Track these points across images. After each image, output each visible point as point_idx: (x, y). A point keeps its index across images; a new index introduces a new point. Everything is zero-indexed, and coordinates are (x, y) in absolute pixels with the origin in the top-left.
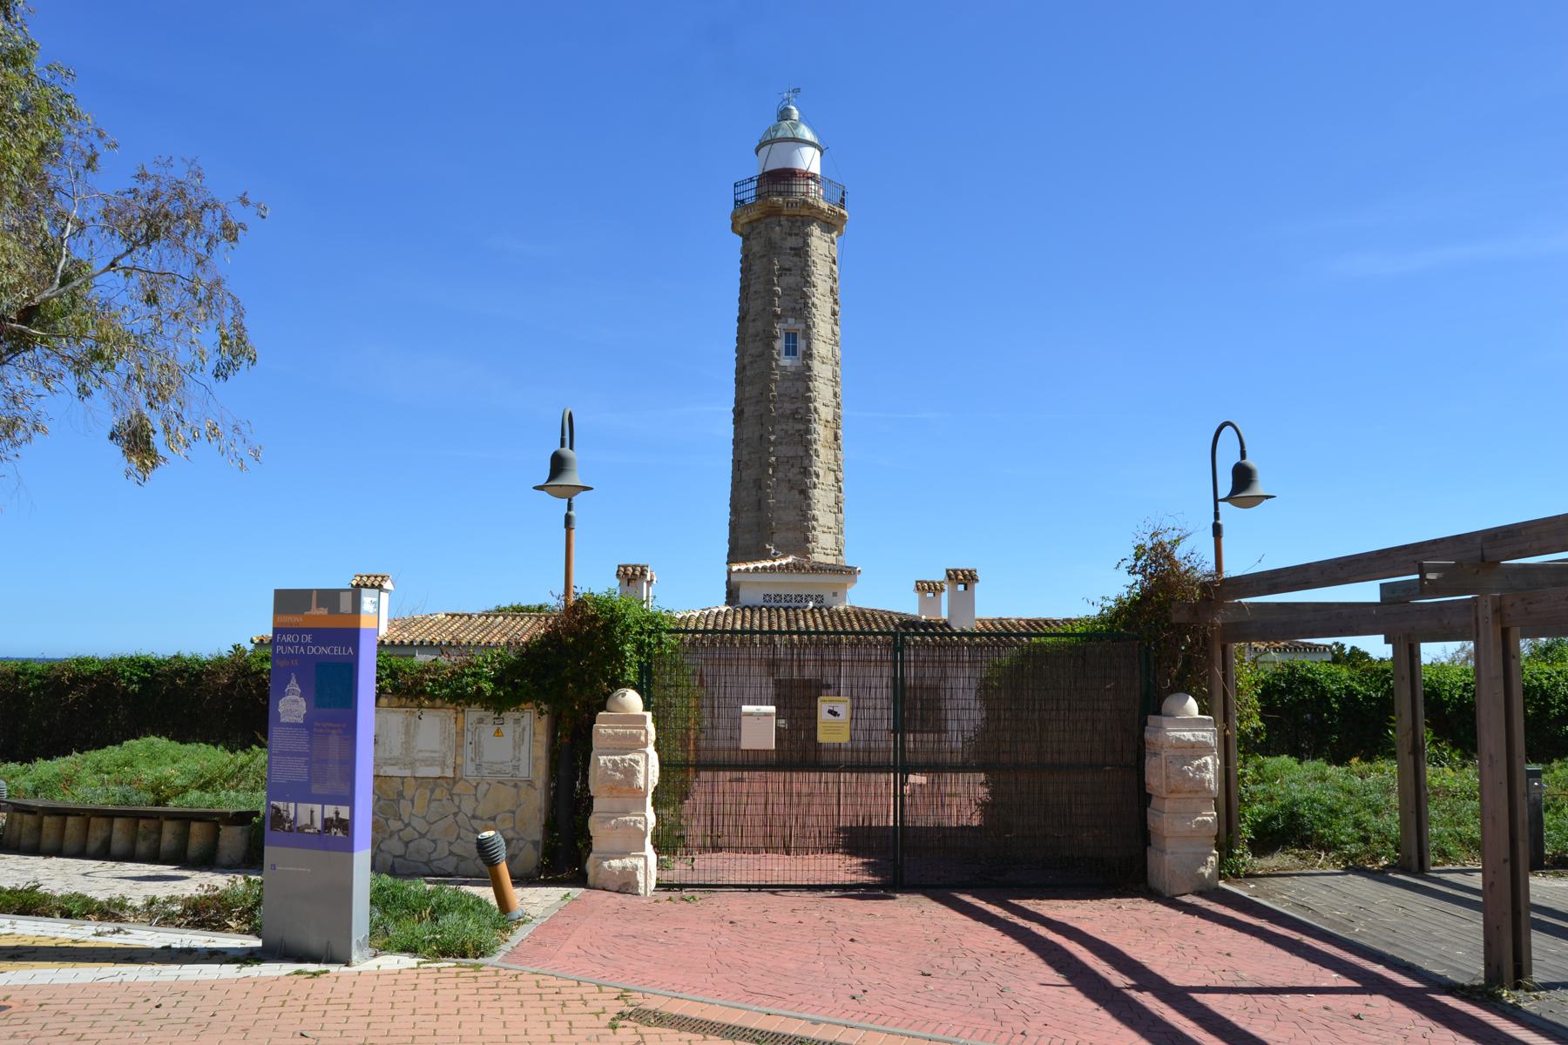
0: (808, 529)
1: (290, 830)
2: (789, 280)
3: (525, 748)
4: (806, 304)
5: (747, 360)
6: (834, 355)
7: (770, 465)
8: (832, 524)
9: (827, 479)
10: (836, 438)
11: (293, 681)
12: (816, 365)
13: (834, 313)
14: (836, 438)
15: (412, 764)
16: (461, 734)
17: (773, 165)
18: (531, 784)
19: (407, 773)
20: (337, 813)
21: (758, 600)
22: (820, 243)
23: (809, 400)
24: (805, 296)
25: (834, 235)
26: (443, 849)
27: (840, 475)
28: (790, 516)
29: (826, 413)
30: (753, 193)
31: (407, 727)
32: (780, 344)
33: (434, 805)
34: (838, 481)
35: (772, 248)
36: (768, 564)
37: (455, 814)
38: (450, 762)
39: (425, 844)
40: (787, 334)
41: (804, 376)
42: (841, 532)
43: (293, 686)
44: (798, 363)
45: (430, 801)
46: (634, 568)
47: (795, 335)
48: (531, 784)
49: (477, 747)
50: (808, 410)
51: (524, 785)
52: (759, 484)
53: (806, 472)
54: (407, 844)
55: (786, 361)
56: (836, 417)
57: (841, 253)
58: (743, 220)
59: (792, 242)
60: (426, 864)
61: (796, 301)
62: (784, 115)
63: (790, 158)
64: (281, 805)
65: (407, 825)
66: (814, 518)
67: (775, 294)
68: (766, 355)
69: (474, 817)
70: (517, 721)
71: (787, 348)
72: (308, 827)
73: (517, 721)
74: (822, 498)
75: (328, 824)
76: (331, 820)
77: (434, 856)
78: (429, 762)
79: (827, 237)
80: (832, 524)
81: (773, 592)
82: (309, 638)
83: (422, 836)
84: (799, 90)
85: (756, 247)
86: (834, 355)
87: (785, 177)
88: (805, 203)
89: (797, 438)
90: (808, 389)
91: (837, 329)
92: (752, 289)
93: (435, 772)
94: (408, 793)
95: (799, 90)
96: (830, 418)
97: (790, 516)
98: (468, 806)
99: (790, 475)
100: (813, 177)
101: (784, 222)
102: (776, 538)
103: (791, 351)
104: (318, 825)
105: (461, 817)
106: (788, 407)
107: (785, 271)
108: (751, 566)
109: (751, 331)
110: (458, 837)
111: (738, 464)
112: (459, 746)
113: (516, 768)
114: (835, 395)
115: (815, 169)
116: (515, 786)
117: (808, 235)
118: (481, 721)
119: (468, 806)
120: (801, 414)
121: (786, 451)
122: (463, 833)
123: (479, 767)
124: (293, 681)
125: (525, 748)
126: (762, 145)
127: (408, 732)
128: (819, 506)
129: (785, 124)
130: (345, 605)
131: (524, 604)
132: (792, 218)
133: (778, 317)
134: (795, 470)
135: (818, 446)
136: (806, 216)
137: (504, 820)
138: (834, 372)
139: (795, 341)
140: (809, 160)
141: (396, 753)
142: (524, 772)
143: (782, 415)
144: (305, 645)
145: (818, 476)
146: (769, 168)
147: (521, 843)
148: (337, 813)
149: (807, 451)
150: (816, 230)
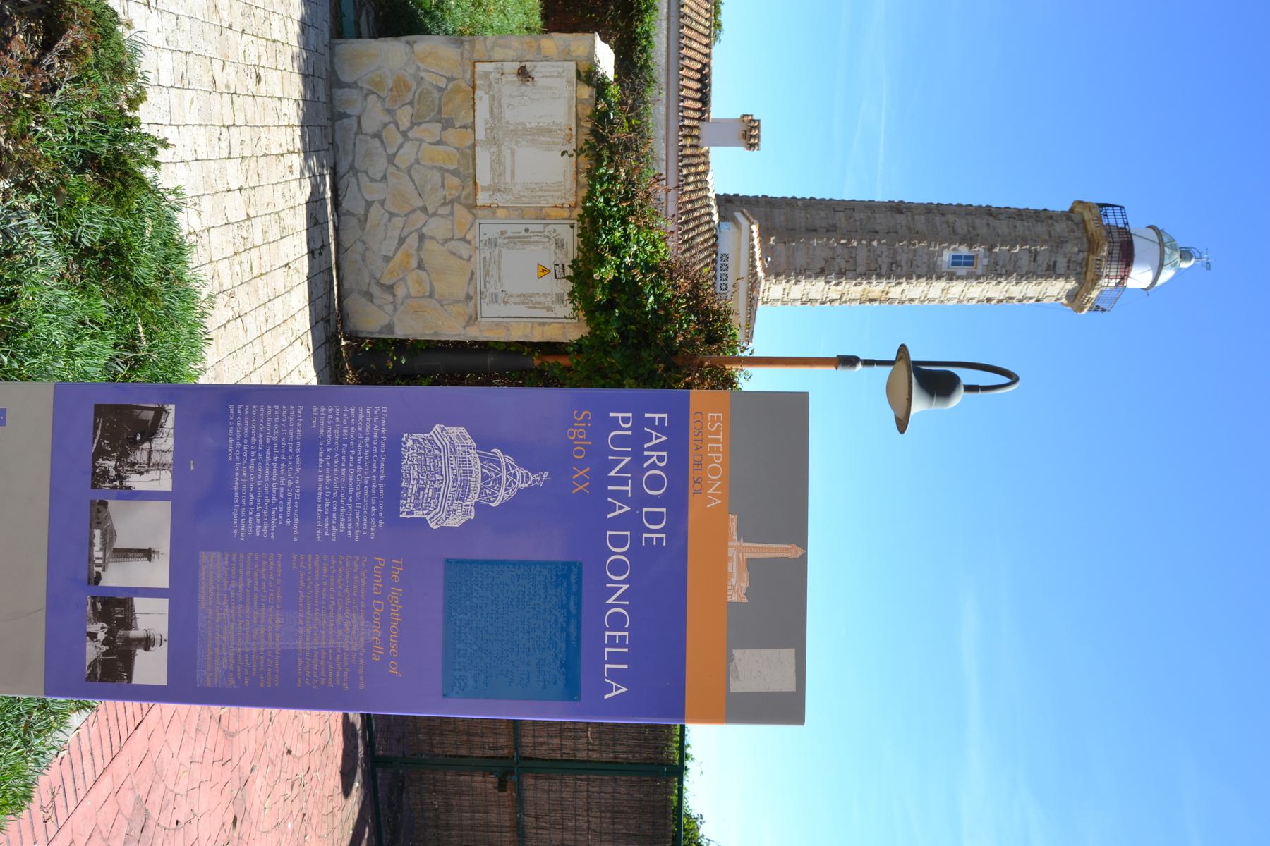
0: (787, 276)
1: (99, 477)
2: (1025, 260)
3: (522, 311)
4: (1000, 275)
5: (950, 218)
6: (949, 299)
7: (849, 241)
8: (791, 296)
9: (834, 292)
10: (871, 300)
11: (526, 479)
12: (942, 284)
13: (989, 300)
14: (871, 300)
15: (493, 141)
16: (541, 215)
17: (1138, 244)
18: (472, 319)
19: (481, 134)
20: (147, 643)
21: (723, 248)
22: (1057, 288)
23: (909, 278)
24: (1008, 275)
25: (1064, 301)
26: (374, 192)
27: (836, 304)
28: (801, 259)
29: (895, 292)
30: (1112, 223)
31: (549, 131)
32: (964, 250)
33: (436, 176)
34: (832, 301)
35: (1058, 243)
36: (757, 256)
37: (424, 209)
38: (499, 199)
39: (379, 166)
40: (972, 257)
41: (932, 273)
42: (784, 303)
43: (514, 479)
44: (945, 268)
45: (442, 170)
46: (757, 136)
47: (972, 264)
48: (472, 319)
49: (521, 241)
50: (899, 277)
51: (470, 310)
52: (831, 230)
53: (841, 274)
54: (377, 136)
55: (947, 256)
56: (890, 301)
57: (1046, 306)
58: (1087, 216)
59: (1062, 263)
60: (352, 167)
61: (1004, 266)
62: (1186, 254)
63: (1143, 261)
64: (164, 442)
65: (404, 134)
66: (797, 282)
67: (1013, 246)
68: (954, 237)
69: (422, 237)
70: (560, 299)
71: (959, 257)
72: (109, 536)
73: (560, 299)
74: (816, 288)
75: (116, 608)
76: (128, 623)
77: (362, 177)
78: (497, 163)
79: (1063, 294)
80: (791, 296)
81: (730, 263)
82: (655, 533)
83: (391, 159)
84: (1209, 268)
85: (1060, 228)
86: (949, 299)
87: (1126, 256)
88: (1099, 277)
89: (873, 266)
90: (919, 277)
91: (974, 302)
92: (1018, 223)
93: (484, 177)
94: (451, 135)
95: (1209, 268)
96: (890, 295)
97: (801, 259)
98: (437, 228)
99: (838, 260)
100: (1123, 278)
101: (1082, 255)
102: (781, 247)
103: (956, 260)
104: (116, 576)
105: (420, 216)
106: (903, 258)
107: (1035, 256)
108: (756, 242)
109: (978, 222)
110: (392, 215)
111: (849, 207)
112: (521, 212)
113: (494, 299)
114: (912, 300)
115: (1131, 283)
116: (469, 297)
117: (1067, 278)
118: (560, 244)
119: (437, 228)
120: (895, 270)
121: (862, 256)
122: (398, 222)
123: (493, 243)
124: (526, 479)
125: (522, 311)
126: (1159, 233)
127: (540, 133)
128: (809, 286)
129: (1177, 256)
130: (756, 670)
131: (722, 8)
132: (1085, 263)
133: (990, 250)
134: (843, 265)
135: (865, 285)
136: (1085, 275)
137: (419, 282)
138: (934, 299)
139: (966, 264)
140: (1140, 277)
141: (509, 114)
142: (488, 309)
143: (895, 252)
144: (632, 522)
145: (837, 285)
146: (1135, 239)
147: (389, 308)
148: (147, 643)
149: (861, 275)
150: (1071, 285)
